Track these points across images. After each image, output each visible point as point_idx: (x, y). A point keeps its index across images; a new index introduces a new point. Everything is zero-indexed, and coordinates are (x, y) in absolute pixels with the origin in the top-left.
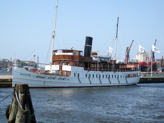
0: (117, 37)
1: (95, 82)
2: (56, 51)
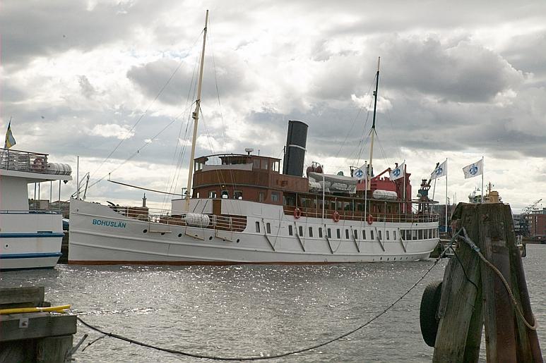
0: (373, 127)
1: (316, 249)
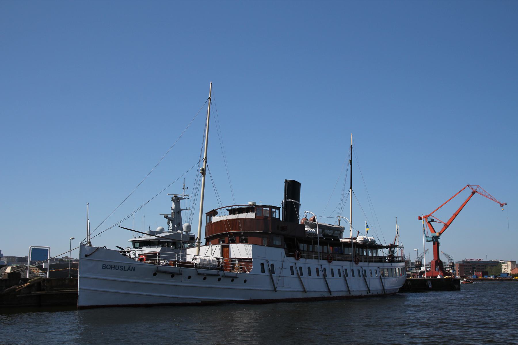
0: (351, 188)
1: (315, 286)
2: (214, 213)
